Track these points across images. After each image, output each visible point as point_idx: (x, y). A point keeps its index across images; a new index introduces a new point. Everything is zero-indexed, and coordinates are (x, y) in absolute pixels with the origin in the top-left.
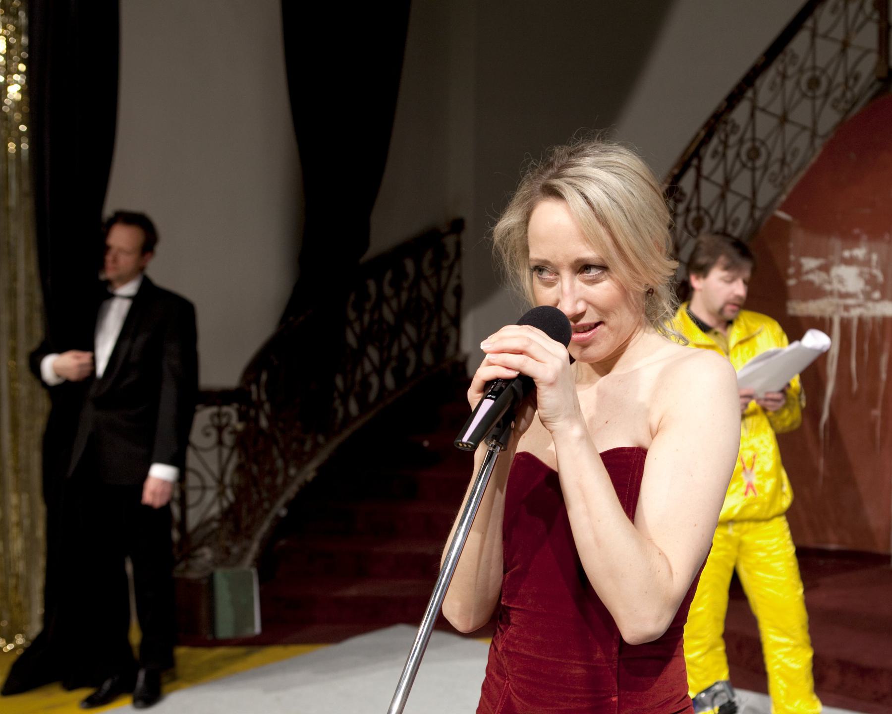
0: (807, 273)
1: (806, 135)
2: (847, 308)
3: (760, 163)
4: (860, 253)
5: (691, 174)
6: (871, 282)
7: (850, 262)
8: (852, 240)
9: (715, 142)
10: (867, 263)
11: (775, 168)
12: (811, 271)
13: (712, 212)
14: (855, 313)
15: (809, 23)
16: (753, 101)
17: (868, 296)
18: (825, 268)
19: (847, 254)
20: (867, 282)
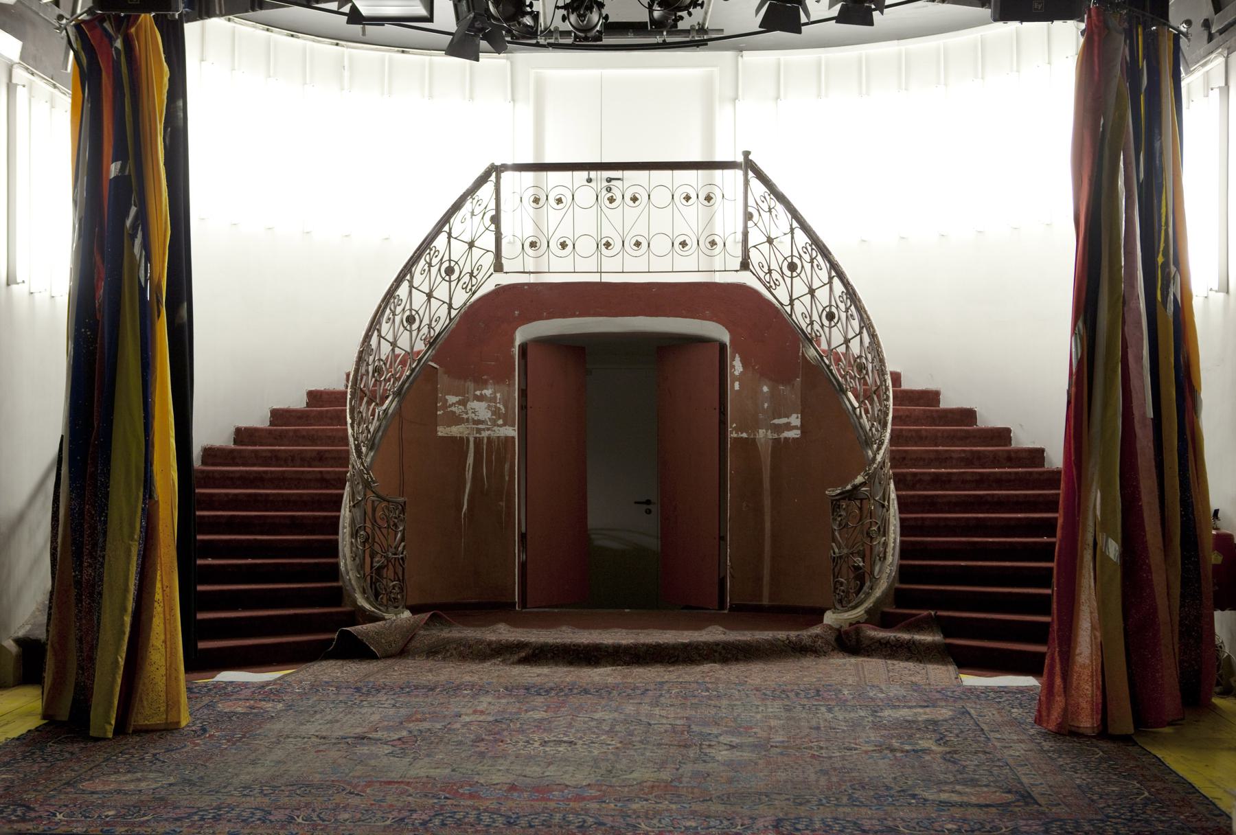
0: (450, 406)
1: (446, 306)
2: (479, 431)
3: (454, 277)
4: (488, 392)
5: (405, 284)
6: (496, 412)
7: (480, 398)
8: (482, 384)
9: (422, 262)
10: (493, 399)
11: (466, 278)
12: (453, 404)
13: (421, 312)
14: (485, 434)
15: (446, 228)
16: (411, 282)
17: (494, 423)
18: (463, 403)
19: (478, 393)
20: (494, 413)
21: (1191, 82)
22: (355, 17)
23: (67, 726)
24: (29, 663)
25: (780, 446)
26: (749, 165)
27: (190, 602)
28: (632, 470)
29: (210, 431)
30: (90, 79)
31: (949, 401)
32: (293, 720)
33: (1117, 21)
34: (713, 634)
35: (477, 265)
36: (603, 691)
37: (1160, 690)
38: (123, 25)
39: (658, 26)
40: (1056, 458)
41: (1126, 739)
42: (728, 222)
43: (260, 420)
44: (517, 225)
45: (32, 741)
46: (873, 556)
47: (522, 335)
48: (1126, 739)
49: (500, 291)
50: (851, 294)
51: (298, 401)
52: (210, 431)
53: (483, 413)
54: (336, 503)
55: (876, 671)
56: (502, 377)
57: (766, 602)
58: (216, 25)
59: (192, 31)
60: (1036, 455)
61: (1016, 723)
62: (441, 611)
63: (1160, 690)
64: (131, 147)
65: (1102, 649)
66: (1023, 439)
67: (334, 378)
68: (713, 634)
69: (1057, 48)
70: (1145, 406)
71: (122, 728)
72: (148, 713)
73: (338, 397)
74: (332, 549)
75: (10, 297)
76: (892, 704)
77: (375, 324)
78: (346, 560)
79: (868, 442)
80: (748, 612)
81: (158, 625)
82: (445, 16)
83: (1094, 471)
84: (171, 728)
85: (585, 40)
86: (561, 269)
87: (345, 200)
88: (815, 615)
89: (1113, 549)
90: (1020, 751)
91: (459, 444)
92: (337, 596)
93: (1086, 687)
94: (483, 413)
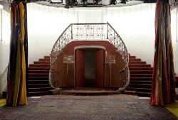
21: (171, 12)
22: (51, 2)
23: (10, 104)
24: (4, 95)
25: (112, 64)
26: (108, 24)
27: (27, 87)
28: (91, 67)
29: (30, 62)
30: (13, 12)
31: (137, 58)
32: (41, 103)
33: (161, 3)
34: (103, 91)
35: (68, 39)
36: (87, 99)
37: (168, 98)
38: (18, 4)
39: (95, 4)
40: (152, 66)
41: (162, 106)
42: (105, 32)
43: (37, 60)
44: (75, 32)
45: (5, 107)
46: (125, 78)
47: (76, 48)
48: (162, 106)
49: (72, 42)
50: (123, 42)
51: (43, 58)
52: (30, 62)
53: (70, 59)
54: (48, 72)
55: (126, 96)
56: (72, 54)
57: (111, 86)
58: (31, 3)
59: (28, 4)
60: (150, 66)
61: (147, 104)
62: (64, 88)
63: (168, 98)
64: (19, 21)
65: (159, 93)
66: (148, 63)
67: (48, 54)
68: (103, 91)
69: (154, 5)
70: (165, 58)
71: (18, 105)
72: (21, 103)
73: (49, 57)
74: (48, 79)
75: (1, 44)
76: (129, 101)
77: (59, 39)
78: (50, 81)
79: (125, 63)
80: (108, 88)
81: (22, 94)
82: (64, 2)
83: (158, 67)
84: (24, 105)
85: (84, 6)
86: (81, 39)
87: (49, 29)
88: (118, 89)
89: (161, 79)
90: (147, 108)
91: (66, 64)
92: (49, 86)
93: (157, 99)
94: (70, 59)
